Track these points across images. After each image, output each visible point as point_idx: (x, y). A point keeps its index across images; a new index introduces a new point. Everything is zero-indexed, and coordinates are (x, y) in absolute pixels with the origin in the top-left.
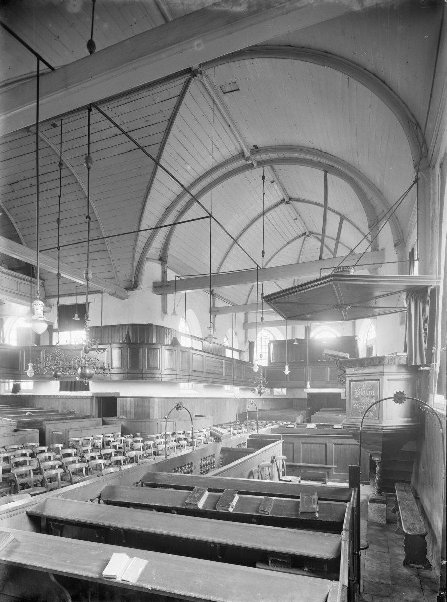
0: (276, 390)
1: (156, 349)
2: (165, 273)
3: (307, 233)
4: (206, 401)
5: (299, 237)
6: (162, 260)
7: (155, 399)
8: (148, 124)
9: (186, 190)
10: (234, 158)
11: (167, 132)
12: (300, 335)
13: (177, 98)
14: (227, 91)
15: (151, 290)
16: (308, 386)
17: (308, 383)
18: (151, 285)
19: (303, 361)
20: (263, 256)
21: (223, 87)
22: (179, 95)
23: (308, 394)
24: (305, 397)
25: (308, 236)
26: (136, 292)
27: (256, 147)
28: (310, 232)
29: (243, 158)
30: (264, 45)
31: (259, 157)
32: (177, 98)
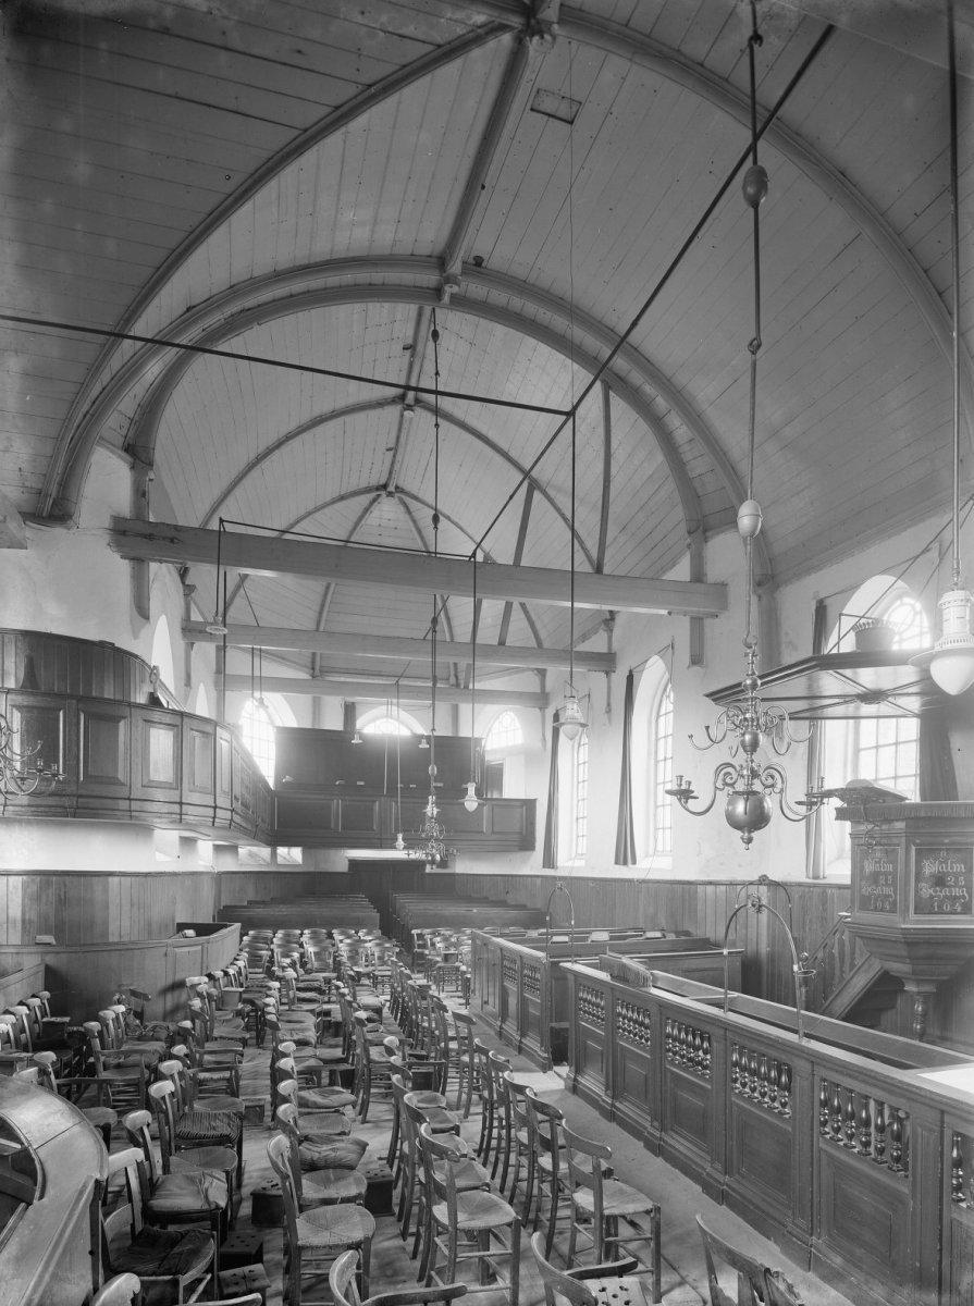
0: (282, 851)
1: (116, 719)
2: (144, 495)
3: (391, 488)
4: (288, 876)
5: (368, 490)
6: (138, 451)
7: (110, 879)
8: (297, 60)
9: (621, 343)
10: (411, 261)
11: (342, 115)
12: (333, 721)
13: (431, 48)
14: (542, 108)
15: (106, 538)
16: (400, 842)
17: (400, 836)
18: (107, 523)
19: (362, 783)
20: (436, 527)
21: (542, 93)
22: (439, 46)
23: (353, 863)
24: (343, 867)
25: (390, 494)
26: (58, 531)
27: (478, 261)
28: (397, 487)
29: (437, 272)
30: (588, 44)
31: (476, 289)
32: (431, 48)
